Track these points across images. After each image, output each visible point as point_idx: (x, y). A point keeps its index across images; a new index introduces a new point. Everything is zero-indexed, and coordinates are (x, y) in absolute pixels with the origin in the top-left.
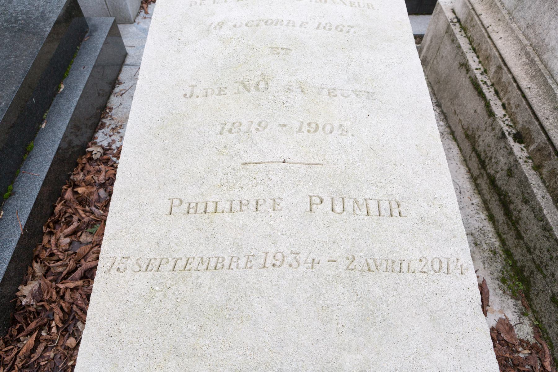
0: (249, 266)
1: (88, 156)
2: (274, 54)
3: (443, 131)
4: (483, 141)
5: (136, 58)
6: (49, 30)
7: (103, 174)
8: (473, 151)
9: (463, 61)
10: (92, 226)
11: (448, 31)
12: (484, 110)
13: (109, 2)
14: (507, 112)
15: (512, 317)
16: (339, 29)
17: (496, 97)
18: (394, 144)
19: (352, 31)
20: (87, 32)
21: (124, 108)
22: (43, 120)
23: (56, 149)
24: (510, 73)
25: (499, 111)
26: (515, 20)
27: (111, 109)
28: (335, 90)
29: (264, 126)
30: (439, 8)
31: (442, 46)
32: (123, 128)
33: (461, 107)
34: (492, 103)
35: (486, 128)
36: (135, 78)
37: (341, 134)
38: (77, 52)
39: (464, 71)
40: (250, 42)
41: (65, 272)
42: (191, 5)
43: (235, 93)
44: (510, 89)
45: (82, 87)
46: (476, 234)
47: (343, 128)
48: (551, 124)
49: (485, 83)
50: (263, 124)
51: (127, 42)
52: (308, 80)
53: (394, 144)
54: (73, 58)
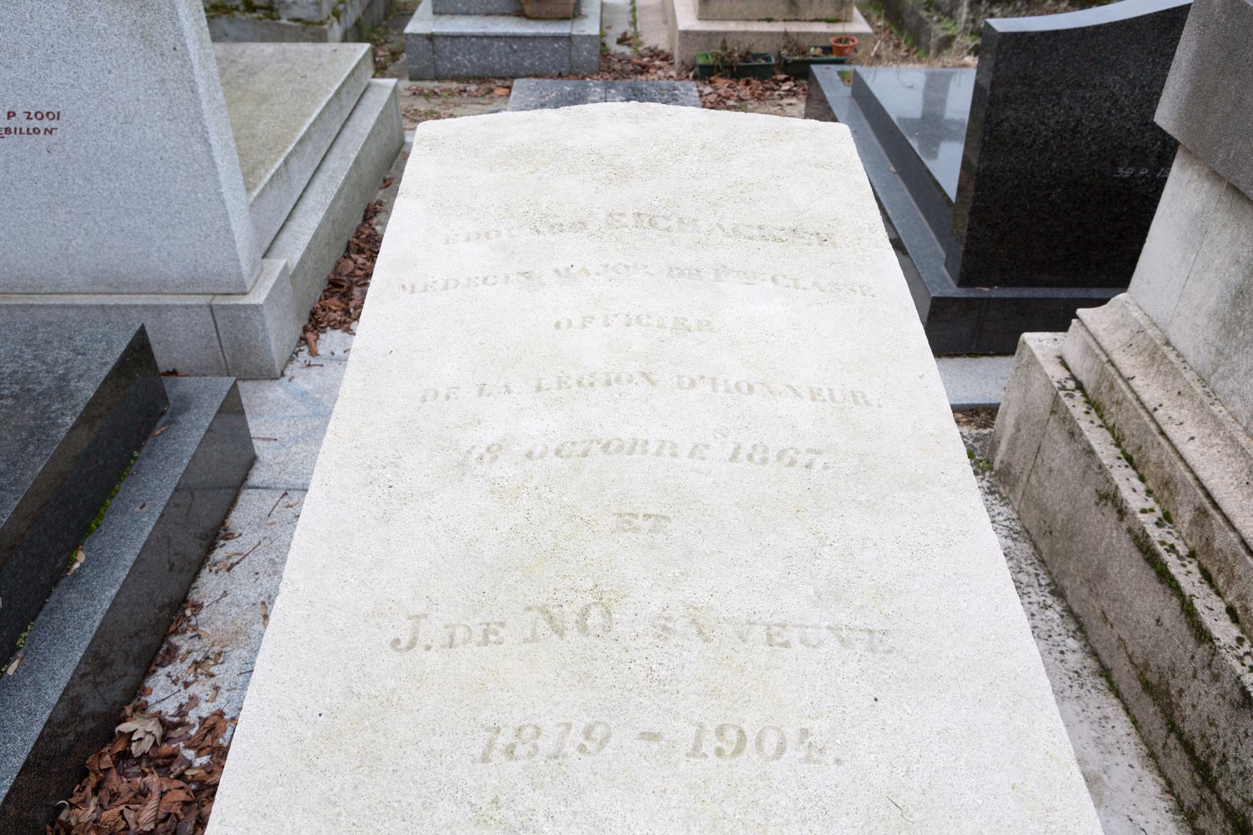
2: (626, 531)
3: (1079, 666)
4: (1194, 706)
5: (277, 468)
6: (70, 420)
7: (152, 803)
8: (1170, 731)
9: (1105, 488)
11: (1056, 407)
12: (1181, 622)
13: (225, 333)
14: (1243, 631)
16: (787, 460)
18: (951, 785)
19: (819, 462)
20: (163, 414)
21: (230, 605)
22: (14, 650)
23: (35, 738)
24: (1234, 529)
26: (1218, 397)
27: (198, 607)
28: (784, 626)
29: (599, 738)
30: (1026, 353)
31: (1045, 443)
32: (222, 663)
33: (1117, 604)
34: (1198, 604)
35: (1195, 670)
36: (270, 521)
37: (808, 759)
38: (130, 465)
39: (1110, 510)
40: (565, 499)
42: (424, 400)
43: (526, 640)
45: (130, 558)
47: (810, 739)
49: (1172, 549)
50: (598, 732)
51: (257, 427)
52: (712, 601)
53: (951, 785)
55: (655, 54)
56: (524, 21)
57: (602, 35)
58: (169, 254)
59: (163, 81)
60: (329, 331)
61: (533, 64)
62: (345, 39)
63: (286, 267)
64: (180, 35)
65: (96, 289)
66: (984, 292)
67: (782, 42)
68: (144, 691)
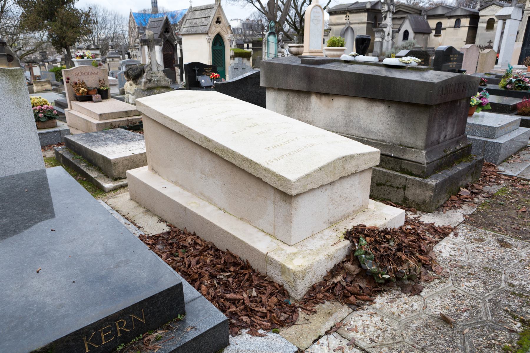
59: (23, 116)
61: (48, 141)
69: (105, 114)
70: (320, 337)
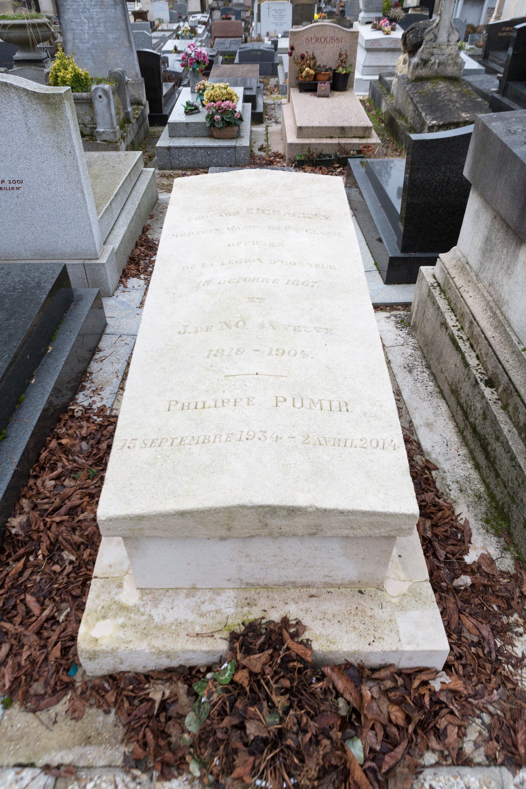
0: (229, 439)
1: (70, 414)
6: (45, 297)
7: (85, 429)
10: (76, 472)
15: (494, 552)
17: (470, 349)
19: (316, 285)
20: (73, 301)
21: (104, 373)
24: (479, 326)
25: (473, 361)
27: (91, 373)
31: (426, 309)
34: (466, 354)
39: (444, 329)
41: (52, 508)
42: (184, 269)
44: (480, 340)
45: (69, 348)
46: (462, 481)
48: (510, 365)
50: (241, 350)
51: (108, 313)
54: (60, 324)
55: (277, 155)
56: (213, 140)
57: (251, 146)
58: (66, 242)
59: (65, 166)
60: (131, 279)
61: (218, 161)
62: (127, 150)
63: (113, 249)
64: (73, 146)
65: (35, 258)
66: (413, 255)
67: (337, 148)
68: (75, 399)
69: (307, 127)
70: (32, 765)
